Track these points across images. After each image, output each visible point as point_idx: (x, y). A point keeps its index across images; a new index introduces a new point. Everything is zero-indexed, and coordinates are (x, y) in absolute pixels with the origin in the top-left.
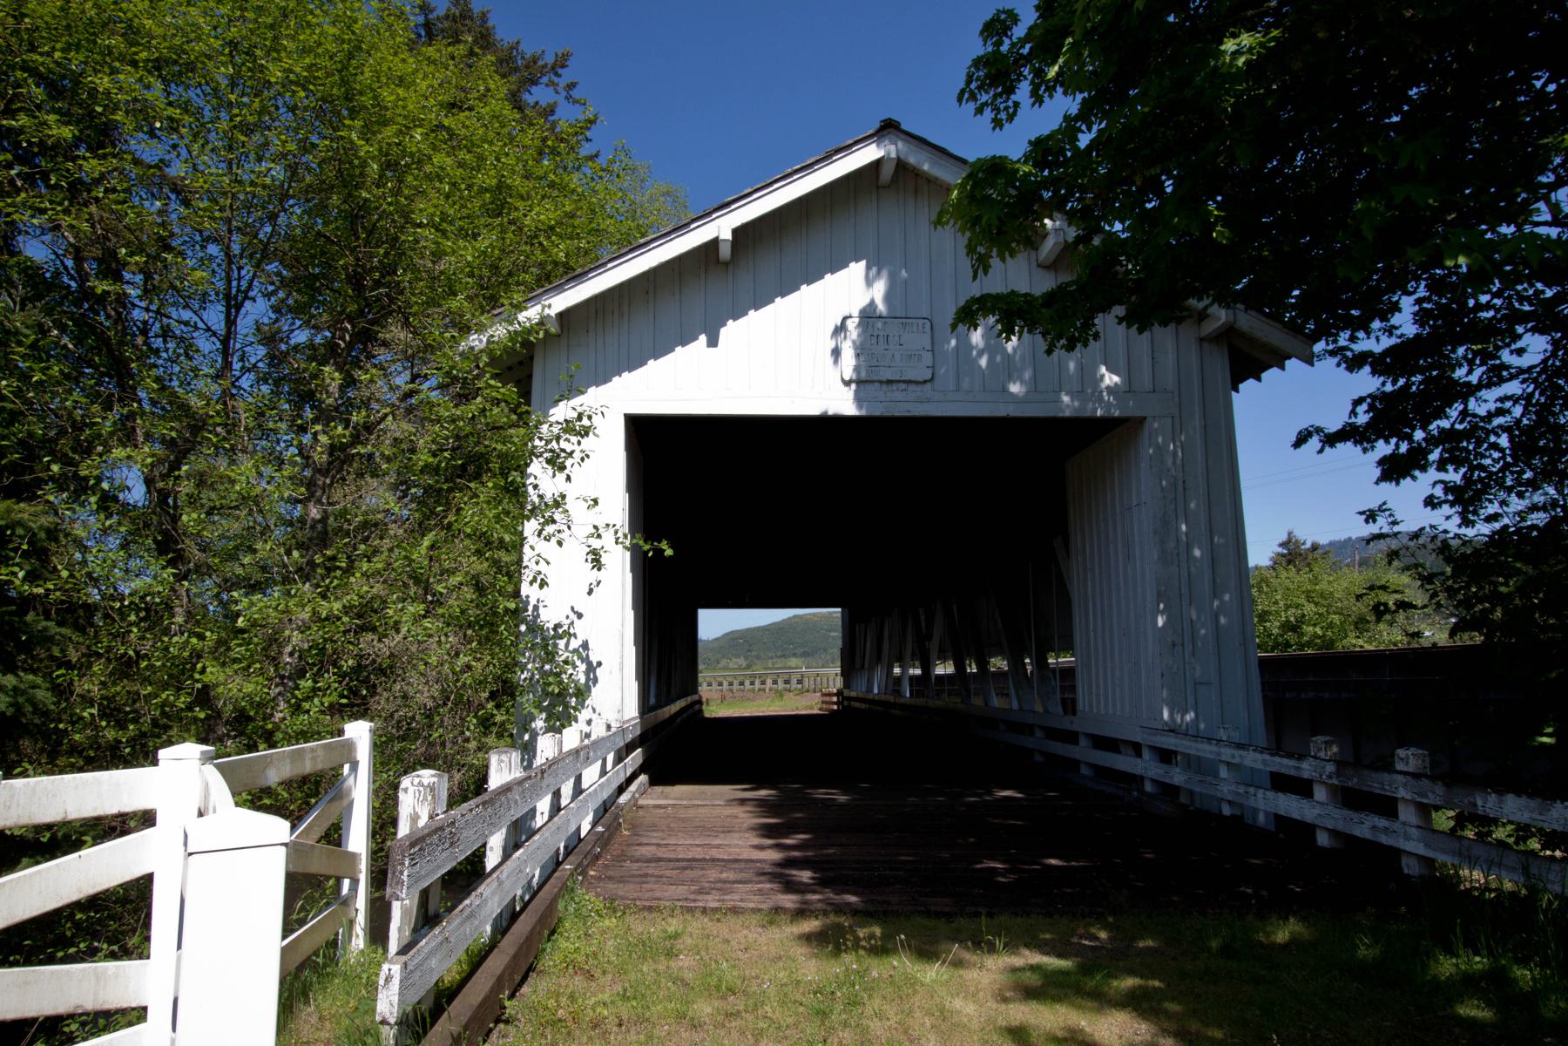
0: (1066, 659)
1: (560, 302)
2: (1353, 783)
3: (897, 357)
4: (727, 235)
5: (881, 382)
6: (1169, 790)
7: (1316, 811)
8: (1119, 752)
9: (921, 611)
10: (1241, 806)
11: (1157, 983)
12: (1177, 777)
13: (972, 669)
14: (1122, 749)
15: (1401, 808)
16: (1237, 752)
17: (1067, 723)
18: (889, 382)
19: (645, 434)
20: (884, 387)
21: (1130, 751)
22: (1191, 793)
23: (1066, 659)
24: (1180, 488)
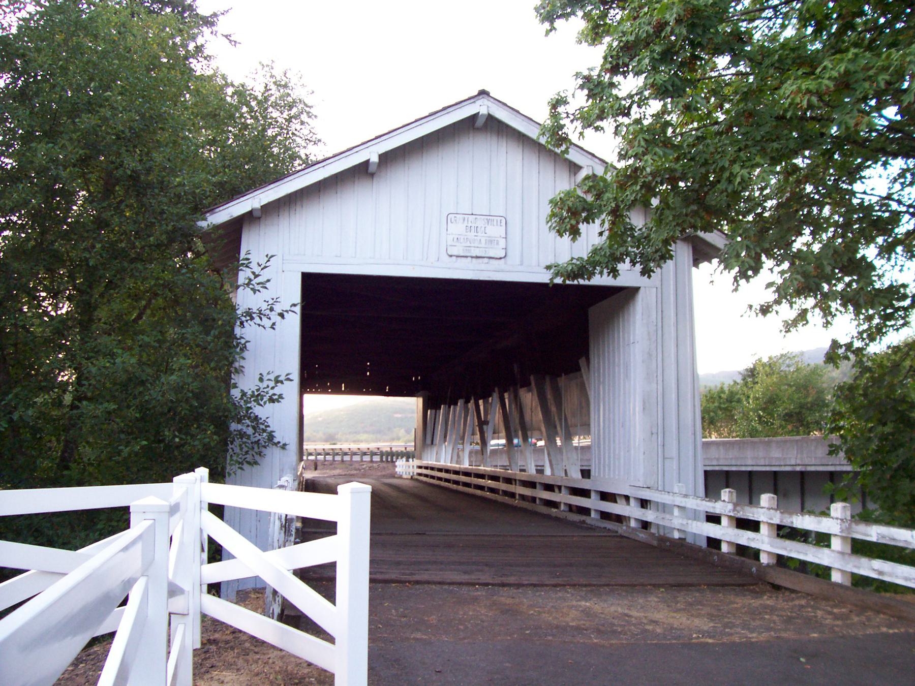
0: (585, 441)
1: (507, 401)
2: (741, 515)
3: (483, 241)
4: (375, 159)
5: (472, 257)
6: (645, 525)
7: (722, 532)
8: (616, 502)
9: (481, 402)
10: (684, 531)
11: (515, 366)
12: (649, 515)
13: (815, 210)
14: (618, 501)
15: (762, 526)
16: (684, 500)
17: (585, 484)
18: (477, 257)
19: (320, 291)
20: (474, 260)
21: (624, 501)
22: (658, 525)
23: (585, 441)
24: (660, 332)
